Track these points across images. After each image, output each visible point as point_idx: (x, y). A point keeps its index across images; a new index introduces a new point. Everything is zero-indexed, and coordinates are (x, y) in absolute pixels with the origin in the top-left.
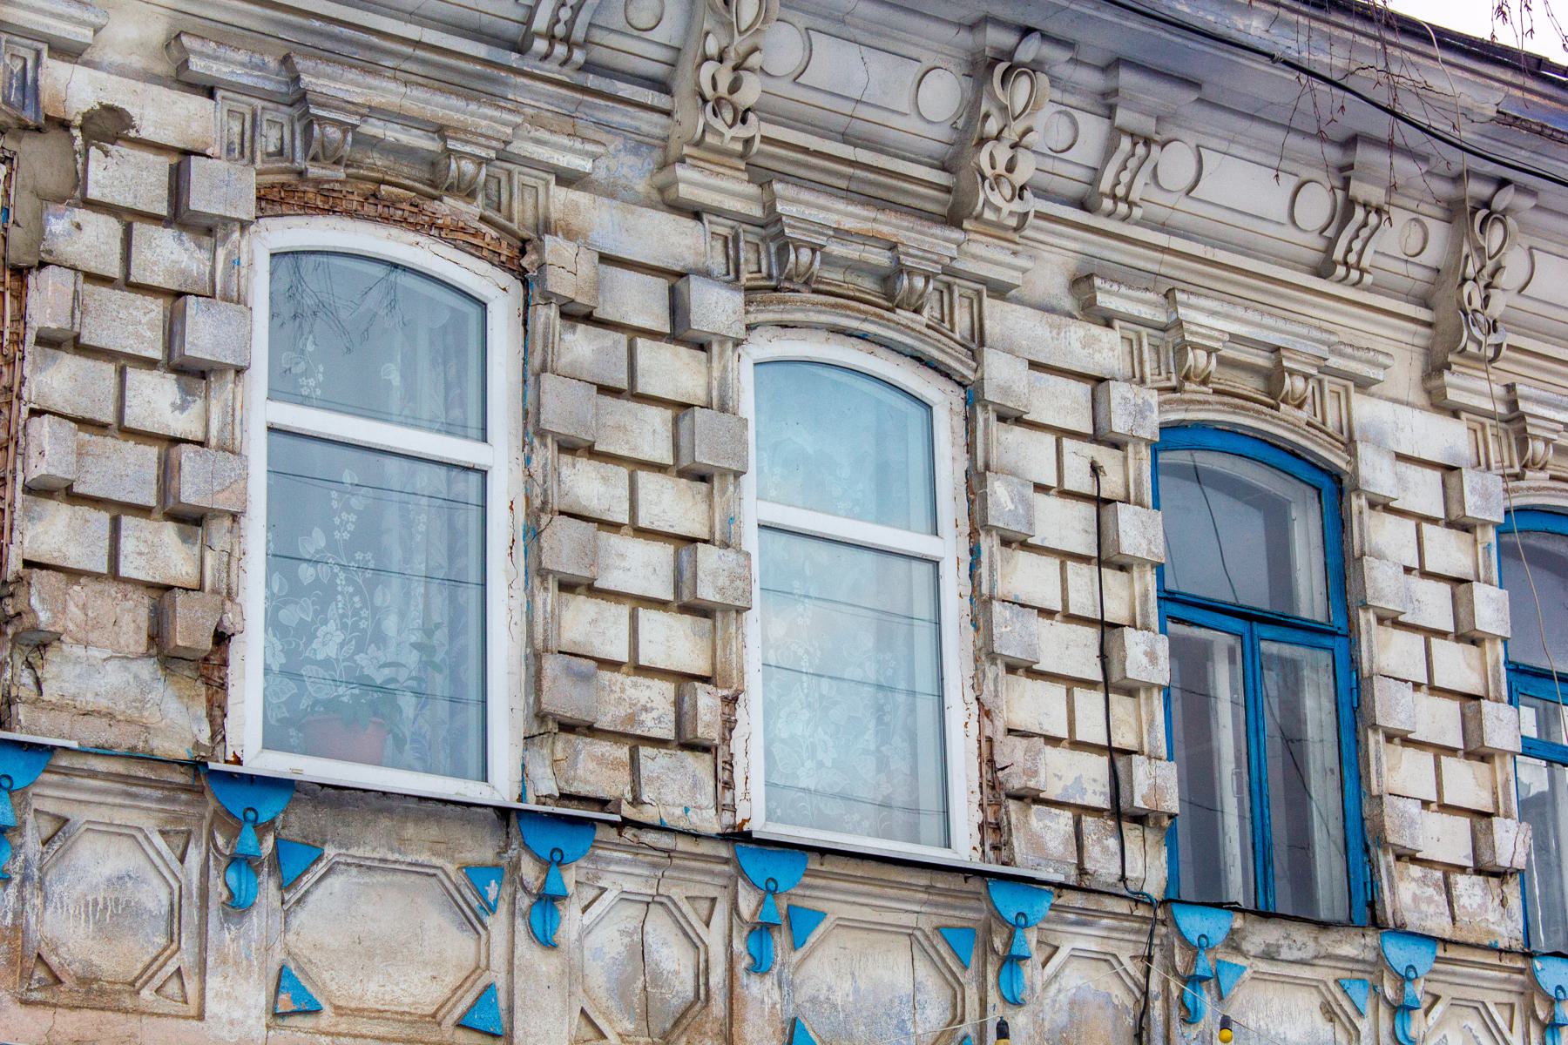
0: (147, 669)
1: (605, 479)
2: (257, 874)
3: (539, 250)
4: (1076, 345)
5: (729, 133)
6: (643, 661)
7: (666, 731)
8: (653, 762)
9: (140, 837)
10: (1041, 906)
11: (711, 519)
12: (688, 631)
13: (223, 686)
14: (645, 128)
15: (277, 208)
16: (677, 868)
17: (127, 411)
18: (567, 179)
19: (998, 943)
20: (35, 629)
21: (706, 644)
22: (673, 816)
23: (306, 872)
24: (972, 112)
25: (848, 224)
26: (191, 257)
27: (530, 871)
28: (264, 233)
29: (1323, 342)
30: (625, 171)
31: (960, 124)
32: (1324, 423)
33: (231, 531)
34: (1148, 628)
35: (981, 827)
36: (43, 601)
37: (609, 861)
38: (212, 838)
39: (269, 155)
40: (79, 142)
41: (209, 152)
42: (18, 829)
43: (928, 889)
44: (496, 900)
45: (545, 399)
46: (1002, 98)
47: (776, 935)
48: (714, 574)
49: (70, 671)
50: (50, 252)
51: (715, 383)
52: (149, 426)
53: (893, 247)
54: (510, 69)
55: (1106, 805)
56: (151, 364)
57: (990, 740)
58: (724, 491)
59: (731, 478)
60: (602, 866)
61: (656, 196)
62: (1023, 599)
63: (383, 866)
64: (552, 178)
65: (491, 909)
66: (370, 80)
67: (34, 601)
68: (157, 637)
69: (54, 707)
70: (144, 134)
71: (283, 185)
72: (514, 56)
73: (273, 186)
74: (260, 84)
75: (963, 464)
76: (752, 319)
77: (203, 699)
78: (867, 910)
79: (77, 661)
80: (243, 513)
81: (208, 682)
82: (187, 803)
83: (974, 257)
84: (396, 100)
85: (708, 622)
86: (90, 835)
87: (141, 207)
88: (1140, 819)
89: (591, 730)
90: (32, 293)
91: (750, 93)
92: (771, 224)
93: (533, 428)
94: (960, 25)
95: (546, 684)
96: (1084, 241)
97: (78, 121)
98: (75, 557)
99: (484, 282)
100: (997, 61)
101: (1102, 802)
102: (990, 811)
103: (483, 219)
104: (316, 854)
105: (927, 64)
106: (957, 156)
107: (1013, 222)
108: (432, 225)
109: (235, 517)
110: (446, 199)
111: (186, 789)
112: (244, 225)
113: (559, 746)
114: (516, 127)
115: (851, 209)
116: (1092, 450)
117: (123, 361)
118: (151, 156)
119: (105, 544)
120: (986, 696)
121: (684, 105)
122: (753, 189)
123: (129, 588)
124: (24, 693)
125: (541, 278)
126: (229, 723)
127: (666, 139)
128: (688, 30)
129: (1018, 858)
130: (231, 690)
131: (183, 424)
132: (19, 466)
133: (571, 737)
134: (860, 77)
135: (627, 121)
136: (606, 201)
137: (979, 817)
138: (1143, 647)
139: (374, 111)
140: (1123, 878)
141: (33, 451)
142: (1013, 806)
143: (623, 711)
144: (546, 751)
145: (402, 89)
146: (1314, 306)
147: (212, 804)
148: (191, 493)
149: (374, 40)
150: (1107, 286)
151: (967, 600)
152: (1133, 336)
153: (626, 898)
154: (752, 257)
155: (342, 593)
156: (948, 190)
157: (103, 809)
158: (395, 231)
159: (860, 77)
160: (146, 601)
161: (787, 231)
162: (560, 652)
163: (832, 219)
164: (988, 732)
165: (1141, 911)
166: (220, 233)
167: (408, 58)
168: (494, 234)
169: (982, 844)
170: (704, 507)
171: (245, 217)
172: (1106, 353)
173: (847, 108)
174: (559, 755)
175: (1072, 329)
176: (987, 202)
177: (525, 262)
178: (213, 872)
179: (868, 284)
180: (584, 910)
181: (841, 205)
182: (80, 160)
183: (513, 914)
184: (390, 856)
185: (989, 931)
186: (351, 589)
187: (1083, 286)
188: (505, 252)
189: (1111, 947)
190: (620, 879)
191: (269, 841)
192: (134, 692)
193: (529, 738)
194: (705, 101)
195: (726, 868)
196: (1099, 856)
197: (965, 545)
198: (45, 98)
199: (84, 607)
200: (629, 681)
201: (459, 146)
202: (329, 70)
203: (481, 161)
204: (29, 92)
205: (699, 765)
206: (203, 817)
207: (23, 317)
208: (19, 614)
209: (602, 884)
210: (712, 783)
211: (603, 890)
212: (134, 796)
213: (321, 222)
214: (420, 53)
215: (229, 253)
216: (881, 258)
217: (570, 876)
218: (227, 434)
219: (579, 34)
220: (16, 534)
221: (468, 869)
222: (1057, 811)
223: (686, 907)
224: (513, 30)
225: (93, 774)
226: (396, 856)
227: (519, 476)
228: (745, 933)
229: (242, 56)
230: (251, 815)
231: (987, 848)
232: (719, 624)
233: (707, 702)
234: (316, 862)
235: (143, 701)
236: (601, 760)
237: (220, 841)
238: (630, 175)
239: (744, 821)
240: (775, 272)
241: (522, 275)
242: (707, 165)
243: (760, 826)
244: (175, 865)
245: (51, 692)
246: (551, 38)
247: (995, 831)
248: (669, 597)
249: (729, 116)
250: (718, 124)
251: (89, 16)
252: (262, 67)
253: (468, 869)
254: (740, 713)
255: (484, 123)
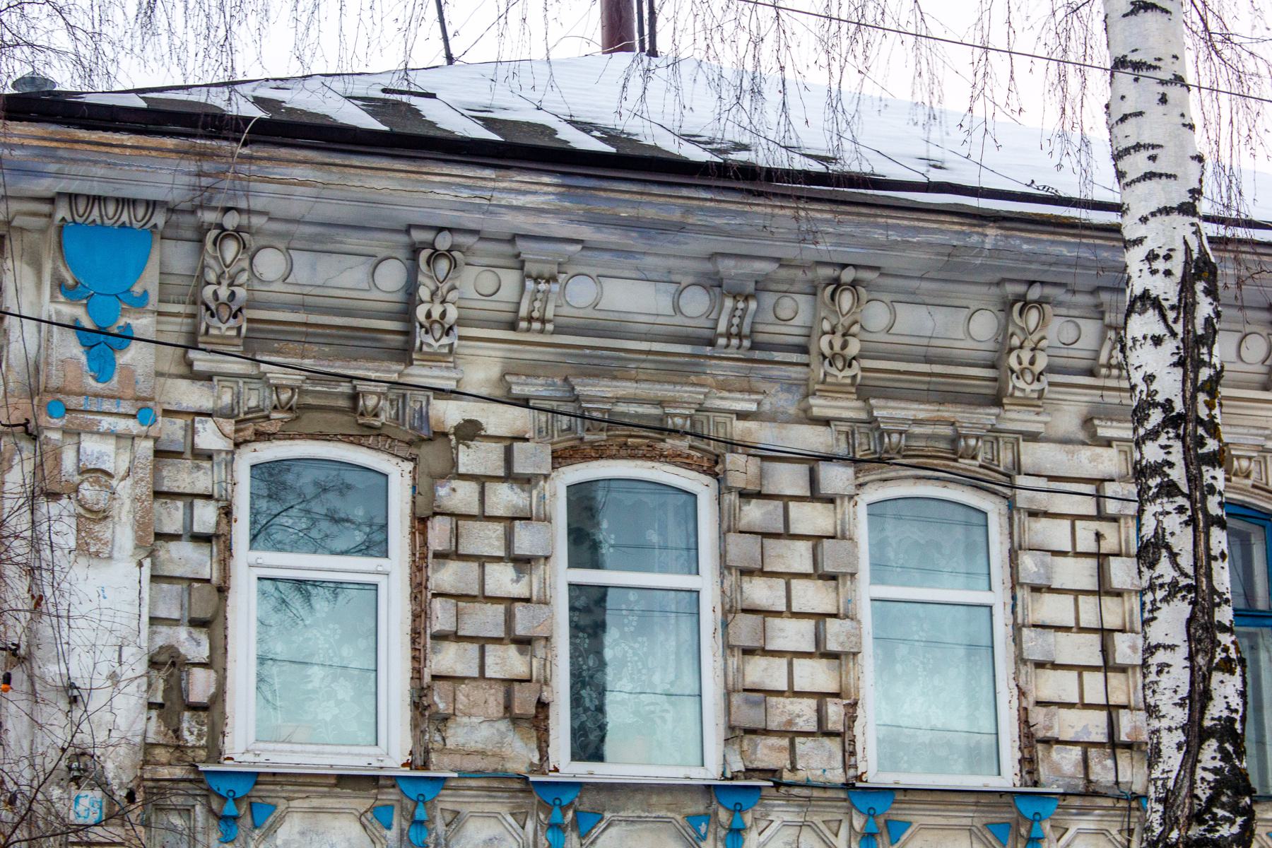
0: (503, 726)
1: (770, 587)
2: (564, 831)
3: (724, 462)
4: (1085, 461)
5: (840, 375)
6: (796, 689)
7: (812, 727)
8: (803, 745)
9: (500, 817)
10: (1051, 806)
11: (838, 601)
12: (825, 669)
13: (547, 730)
14: (794, 375)
15: (569, 461)
16: (814, 806)
17: (486, 587)
18: (742, 416)
19: (1023, 831)
20: (437, 713)
21: (836, 674)
22: (815, 775)
23: (594, 827)
24: (1004, 334)
25: (921, 415)
26: (519, 497)
27: (723, 816)
28: (562, 476)
29: (1261, 436)
30: (782, 403)
31: (1000, 339)
32: (1267, 484)
33: (545, 647)
34: (1132, 631)
35: (1020, 761)
36: (441, 698)
37: (774, 806)
38: (538, 815)
39: (563, 431)
40: (454, 442)
41: (527, 436)
42: (432, 820)
43: (976, 804)
44: (706, 833)
45: (728, 548)
46: (1021, 324)
47: (879, 839)
48: (837, 635)
49: (461, 732)
50: (439, 507)
51: (839, 522)
52: (499, 594)
53: (953, 424)
54: (707, 357)
55: (1105, 740)
56: (499, 559)
57: (1026, 709)
58: (844, 584)
59: (849, 578)
60: (769, 808)
61: (802, 415)
62: (1048, 622)
63: (639, 820)
64: (734, 417)
65: (704, 838)
66: (615, 383)
67: (436, 698)
68: (508, 707)
69: (451, 752)
70: (490, 432)
71: (572, 447)
72: (709, 348)
73: (566, 449)
74: (554, 394)
75: (1007, 545)
76: (861, 480)
77: (535, 739)
78: (939, 818)
79: (465, 725)
80: (551, 637)
81: (537, 728)
82: (523, 798)
83: (1010, 420)
84: (632, 391)
85: (837, 662)
86: (474, 819)
87: (489, 473)
88: (1128, 746)
89: (766, 732)
90: (430, 531)
91: (854, 348)
92: (872, 421)
93: (725, 567)
94: (990, 284)
95: (733, 710)
96: (1091, 395)
97: (452, 430)
98: (460, 670)
99: (695, 483)
100: (1015, 301)
101: (1103, 738)
102: (1026, 751)
103: (691, 447)
104: (600, 817)
105: (973, 308)
106: (999, 358)
107: (1035, 395)
108: (661, 455)
109: (547, 639)
110: (667, 440)
111: (522, 791)
112: (546, 477)
113: (745, 742)
114: (706, 395)
115: (922, 407)
116: (1096, 525)
117: (482, 560)
118: (494, 444)
119: (477, 661)
120: (1021, 684)
121: (814, 359)
122: (859, 404)
123: (493, 682)
124: (436, 746)
125: (725, 479)
126: (550, 750)
127: (807, 380)
128: (814, 316)
129: (1043, 778)
130: (551, 732)
131: (519, 590)
132: (428, 624)
133: (753, 737)
134: (930, 324)
135: (783, 374)
136: (768, 424)
137: (1019, 755)
138: (1128, 644)
139: (618, 400)
140: (1117, 783)
141: (434, 618)
142: (1040, 747)
143: (784, 719)
144: (736, 747)
145: (635, 385)
146: (1262, 409)
147: (537, 798)
148: (520, 630)
149: (623, 354)
150: (1103, 423)
151: (1010, 627)
152: (1126, 449)
153: (786, 824)
154: (864, 440)
155: (630, 661)
156: (995, 380)
157: (478, 805)
158: (639, 462)
159: (930, 324)
160: (502, 688)
161: (882, 425)
162: (745, 690)
163: (910, 414)
164: (1024, 704)
165: (1122, 804)
166: (533, 482)
167: (644, 361)
168: (699, 455)
169: (1021, 771)
170: (834, 595)
171: (545, 472)
172: (1107, 463)
173: (925, 342)
174: (745, 748)
175: (1083, 452)
176: (1014, 387)
177: (717, 469)
178: (540, 833)
179: (943, 445)
180: (760, 834)
181: (915, 406)
182: (454, 452)
183: (715, 840)
184: (643, 815)
185: (1018, 824)
186: (636, 658)
187: (1089, 424)
188: (706, 464)
189: (1104, 826)
190: (782, 815)
191: (570, 814)
192: (497, 738)
193: (726, 740)
194: (825, 357)
195: (844, 804)
196: (1100, 771)
197: (1009, 594)
198: (432, 422)
199: (467, 696)
200: (787, 701)
201: (672, 411)
202: (591, 382)
203: (685, 417)
204: (424, 419)
205: (834, 745)
206: (533, 803)
207: (426, 544)
208: (429, 706)
209: (770, 818)
210: (841, 754)
211: (772, 821)
212: (495, 797)
213: (595, 464)
214: (650, 357)
215: (539, 493)
216: (947, 431)
217: (748, 818)
218: (542, 594)
219: (746, 330)
220: (428, 662)
221: (688, 817)
222: (1071, 747)
223: (822, 827)
224: (708, 333)
225: (470, 788)
226: (647, 814)
227: (718, 592)
228: (859, 839)
229: (541, 381)
230: (558, 802)
231: (1024, 773)
232: (843, 662)
233: (835, 711)
234: (600, 821)
235: (502, 743)
236: (772, 748)
237: (542, 816)
238: (785, 404)
239: (863, 773)
240: (878, 449)
241: (715, 475)
242: (830, 394)
243: (875, 777)
244: (520, 830)
245: (450, 743)
246: (729, 336)
247: (1028, 763)
248: (813, 650)
249: (840, 365)
250: (833, 371)
251: (453, 374)
252: (554, 384)
253: (688, 817)
254: (859, 712)
255: (686, 395)
